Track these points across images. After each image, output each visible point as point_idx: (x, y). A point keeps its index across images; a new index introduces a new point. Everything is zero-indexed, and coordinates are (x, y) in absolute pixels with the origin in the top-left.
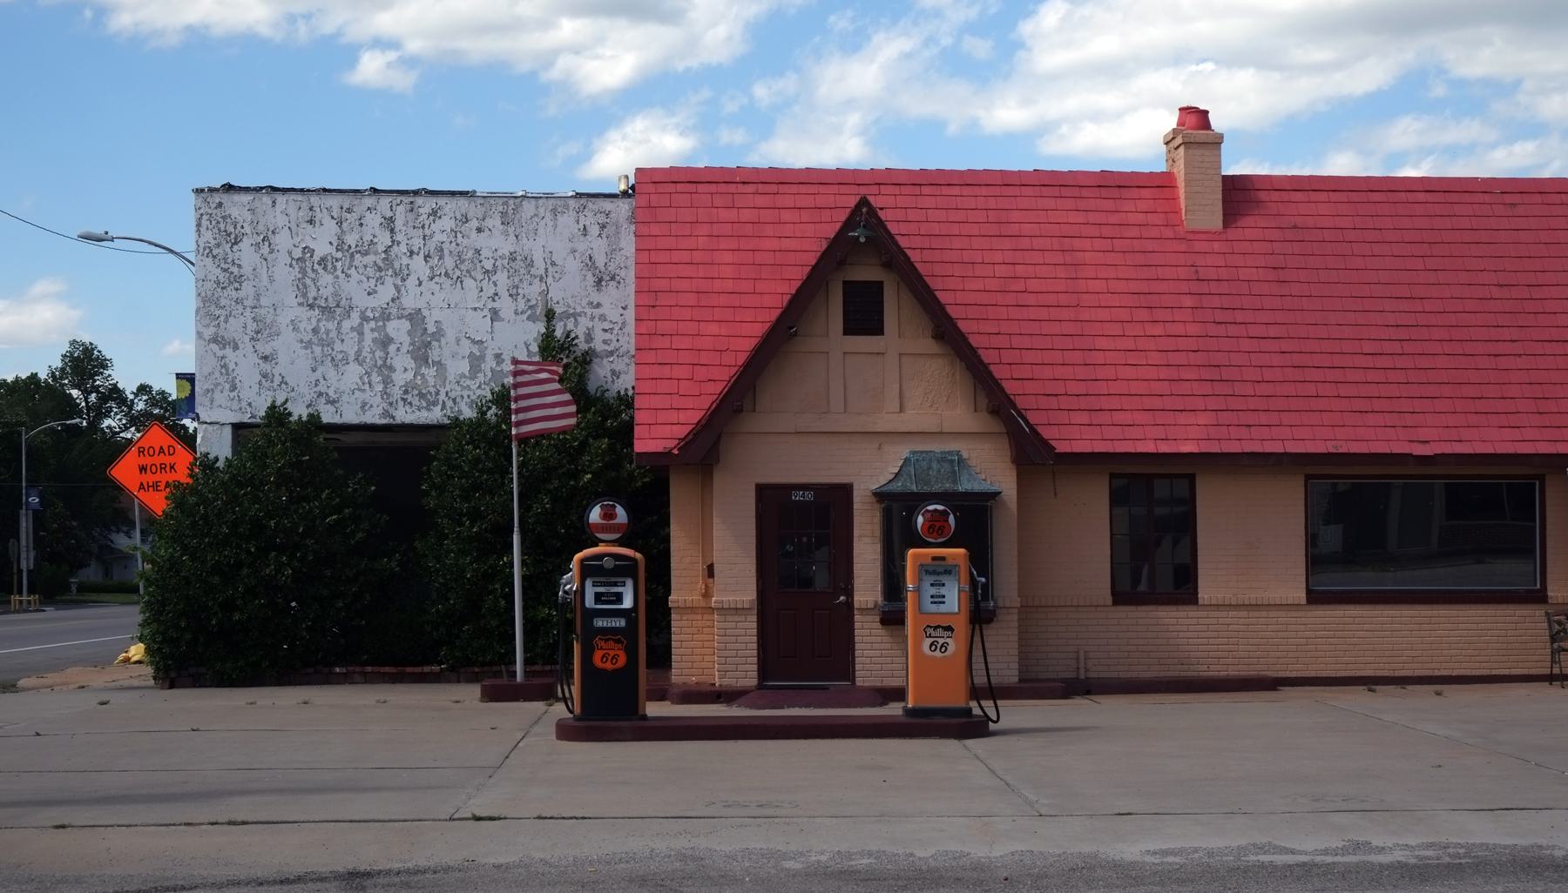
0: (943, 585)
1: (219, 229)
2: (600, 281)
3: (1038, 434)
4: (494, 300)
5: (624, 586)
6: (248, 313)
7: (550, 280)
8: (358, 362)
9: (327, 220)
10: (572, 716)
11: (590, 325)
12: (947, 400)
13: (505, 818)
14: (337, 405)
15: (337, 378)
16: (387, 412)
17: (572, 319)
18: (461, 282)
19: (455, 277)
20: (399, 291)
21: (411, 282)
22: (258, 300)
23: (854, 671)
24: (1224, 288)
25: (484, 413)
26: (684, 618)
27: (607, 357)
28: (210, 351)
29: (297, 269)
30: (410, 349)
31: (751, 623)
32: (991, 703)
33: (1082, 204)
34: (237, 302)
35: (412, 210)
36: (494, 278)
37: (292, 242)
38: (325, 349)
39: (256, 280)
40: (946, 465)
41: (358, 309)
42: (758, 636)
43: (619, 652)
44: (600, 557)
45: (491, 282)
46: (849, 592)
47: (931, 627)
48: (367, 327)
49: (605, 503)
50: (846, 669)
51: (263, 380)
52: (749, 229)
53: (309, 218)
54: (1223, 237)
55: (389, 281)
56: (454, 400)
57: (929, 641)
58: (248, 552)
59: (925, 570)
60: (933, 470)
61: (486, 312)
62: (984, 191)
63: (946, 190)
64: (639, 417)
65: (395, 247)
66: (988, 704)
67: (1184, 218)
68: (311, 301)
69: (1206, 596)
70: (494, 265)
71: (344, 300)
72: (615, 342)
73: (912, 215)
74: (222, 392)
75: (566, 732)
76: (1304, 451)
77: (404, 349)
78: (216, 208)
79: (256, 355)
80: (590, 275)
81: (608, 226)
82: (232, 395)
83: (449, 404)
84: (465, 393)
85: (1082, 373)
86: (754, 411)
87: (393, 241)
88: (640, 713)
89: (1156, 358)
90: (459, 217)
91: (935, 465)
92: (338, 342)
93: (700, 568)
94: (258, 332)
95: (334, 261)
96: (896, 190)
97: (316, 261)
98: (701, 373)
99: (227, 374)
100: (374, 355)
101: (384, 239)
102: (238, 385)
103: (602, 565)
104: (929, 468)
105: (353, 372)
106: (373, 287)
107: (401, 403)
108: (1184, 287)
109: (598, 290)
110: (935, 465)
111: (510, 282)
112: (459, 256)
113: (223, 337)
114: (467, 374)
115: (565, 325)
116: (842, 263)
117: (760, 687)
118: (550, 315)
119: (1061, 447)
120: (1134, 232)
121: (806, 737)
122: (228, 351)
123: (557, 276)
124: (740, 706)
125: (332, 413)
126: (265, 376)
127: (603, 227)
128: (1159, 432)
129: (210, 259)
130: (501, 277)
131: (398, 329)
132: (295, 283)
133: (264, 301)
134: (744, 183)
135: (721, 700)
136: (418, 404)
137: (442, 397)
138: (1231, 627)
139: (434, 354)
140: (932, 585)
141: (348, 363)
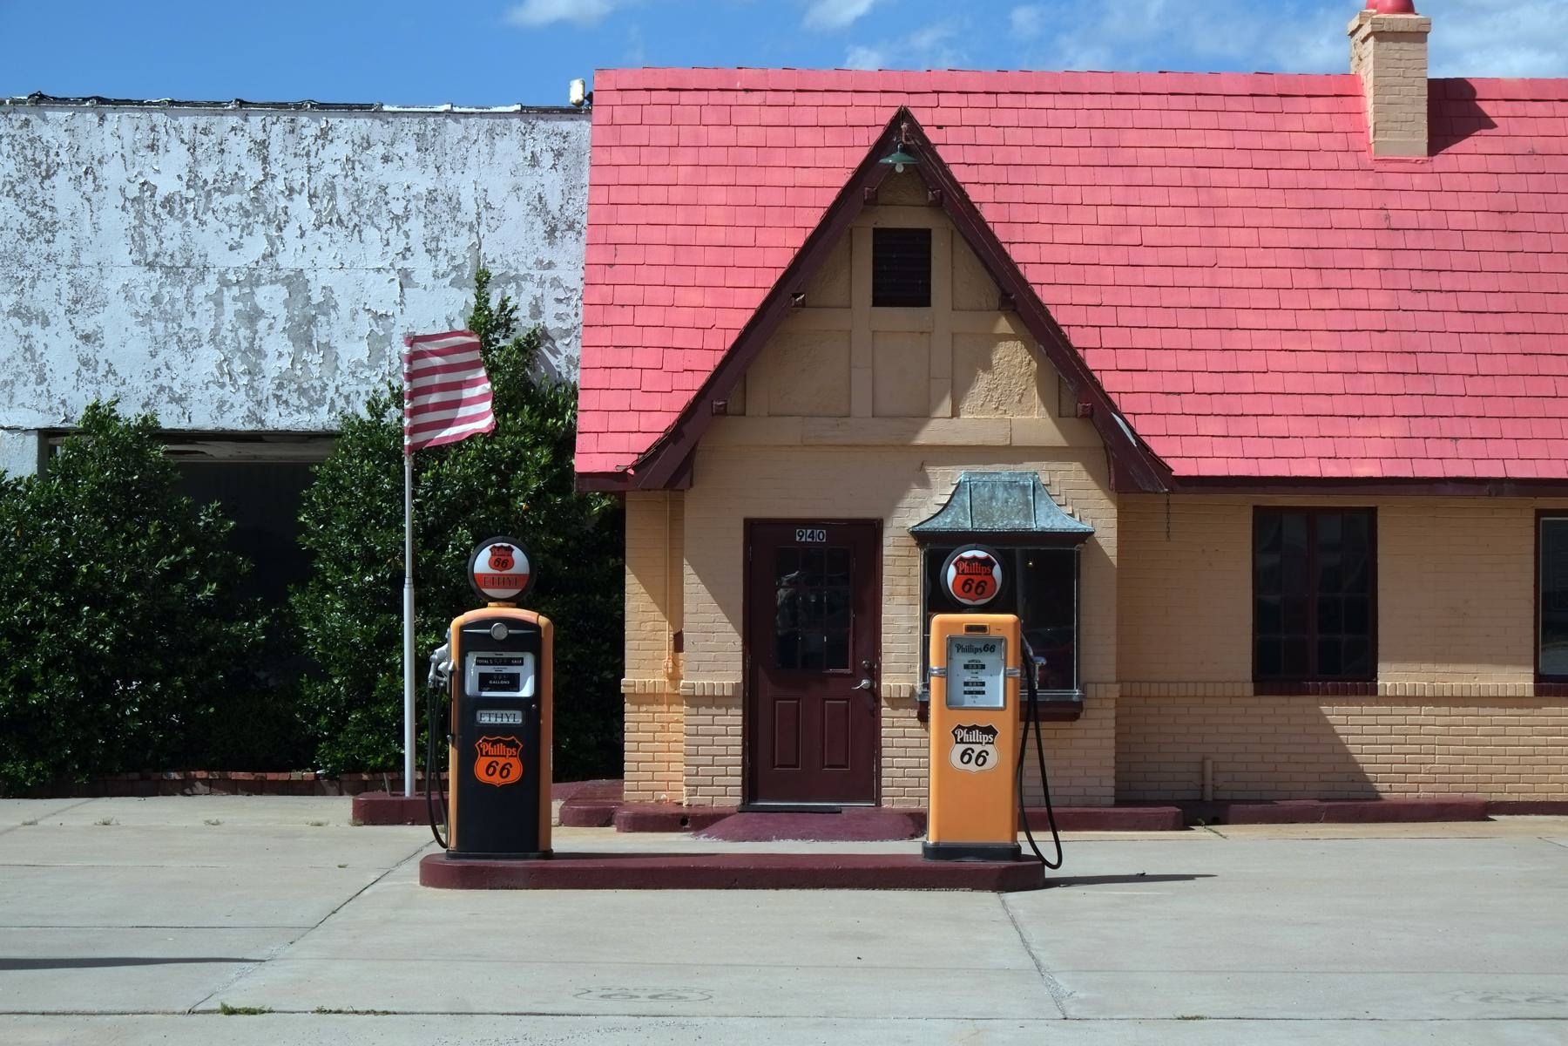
0: (983, 667)
1: (25, 158)
2: (553, 230)
3: (1147, 449)
4: (404, 258)
5: (522, 664)
6: (63, 275)
7: (483, 230)
8: (215, 343)
9: (174, 144)
10: (444, 850)
11: (538, 292)
12: (1020, 401)
13: (270, 1011)
14: (184, 404)
15: (185, 366)
16: (255, 414)
17: (514, 285)
18: (360, 232)
19: (351, 225)
20: (272, 244)
21: (291, 232)
22: (78, 257)
23: (879, 786)
24: (1427, 240)
25: (380, 415)
26: (644, 708)
27: (562, 338)
28: (9, 328)
29: (133, 214)
30: (287, 326)
31: (733, 720)
32: (1049, 835)
33: (1227, 121)
34: (48, 259)
35: (292, 131)
36: (406, 227)
37: (126, 175)
38: (170, 326)
39: (75, 228)
40: (1016, 493)
41: (216, 270)
42: (744, 735)
43: (510, 760)
44: (486, 623)
45: (401, 231)
46: (874, 674)
47: (963, 728)
48: (228, 295)
49: (498, 545)
50: (866, 784)
51: (83, 369)
52: (750, 156)
53: (150, 142)
54: (1428, 167)
55: (259, 230)
56: (347, 398)
57: (961, 748)
58: (53, 609)
59: (954, 645)
60: (997, 500)
61: (393, 274)
62: (1087, 101)
63: (1032, 101)
64: (583, 422)
65: (269, 183)
66: (1043, 839)
67: (1371, 140)
68: (150, 258)
69: (1389, 684)
70: (406, 208)
71: (197, 255)
72: (573, 317)
73: (983, 136)
74: (25, 385)
75: (434, 874)
76: (1534, 475)
77: (279, 327)
78: (21, 127)
79: (73, 332)
80: (539, 221)
81: (566, 154)
82: (39, 389)
83: (340, 403)
84: (363, 388)
85: (1216, 361)
86: (744, 414)
87: (266, 175)
88: (542, 847)
89: (1325, 341)
90: (358, 140)
91: (1000, 494)
92: (187, 316)
93: (667, 636)
94: (76, 302)
95: (184, 201)
96: (962, 100)
97: (158, 203)
98: (675, 360)
99: (33, 360)
100: (236, 334)
101: (254, 171)
102: (49, 375)
103: (489, 635)
104: (991, 498)
105: (208, 358)
106: (237, 239)
107: (273, 402)
108: (1368, 239)
109: (549, 244)
110: (1000, 494)
111: (428, 233)
112: (358, 196)
113: (28, 309)
114: (366, 361)
115: (503, 293)
116: (873, 201)
117: (746, 807)
118: (482, 281)
119: (1180, 468)
120: (1300, 160)
121: (777, 887)
122: (35, 329)
123: (493, 224)
124: (709, 837)
125: (178, 416)
126: (85, 363)
127: (559, 154)
128: (1326, 448)
129: (12, 199)
130: (416, 226)
131: (271, 298)
132: (129, 234)
133: (86, 258)
134: (746, 90)
135: (687, 826)
136: (297, 403)
137: (330, 393)
138: (1424, 729)
139: (320, 334)
140: (966, 667)
141: (200, 346)
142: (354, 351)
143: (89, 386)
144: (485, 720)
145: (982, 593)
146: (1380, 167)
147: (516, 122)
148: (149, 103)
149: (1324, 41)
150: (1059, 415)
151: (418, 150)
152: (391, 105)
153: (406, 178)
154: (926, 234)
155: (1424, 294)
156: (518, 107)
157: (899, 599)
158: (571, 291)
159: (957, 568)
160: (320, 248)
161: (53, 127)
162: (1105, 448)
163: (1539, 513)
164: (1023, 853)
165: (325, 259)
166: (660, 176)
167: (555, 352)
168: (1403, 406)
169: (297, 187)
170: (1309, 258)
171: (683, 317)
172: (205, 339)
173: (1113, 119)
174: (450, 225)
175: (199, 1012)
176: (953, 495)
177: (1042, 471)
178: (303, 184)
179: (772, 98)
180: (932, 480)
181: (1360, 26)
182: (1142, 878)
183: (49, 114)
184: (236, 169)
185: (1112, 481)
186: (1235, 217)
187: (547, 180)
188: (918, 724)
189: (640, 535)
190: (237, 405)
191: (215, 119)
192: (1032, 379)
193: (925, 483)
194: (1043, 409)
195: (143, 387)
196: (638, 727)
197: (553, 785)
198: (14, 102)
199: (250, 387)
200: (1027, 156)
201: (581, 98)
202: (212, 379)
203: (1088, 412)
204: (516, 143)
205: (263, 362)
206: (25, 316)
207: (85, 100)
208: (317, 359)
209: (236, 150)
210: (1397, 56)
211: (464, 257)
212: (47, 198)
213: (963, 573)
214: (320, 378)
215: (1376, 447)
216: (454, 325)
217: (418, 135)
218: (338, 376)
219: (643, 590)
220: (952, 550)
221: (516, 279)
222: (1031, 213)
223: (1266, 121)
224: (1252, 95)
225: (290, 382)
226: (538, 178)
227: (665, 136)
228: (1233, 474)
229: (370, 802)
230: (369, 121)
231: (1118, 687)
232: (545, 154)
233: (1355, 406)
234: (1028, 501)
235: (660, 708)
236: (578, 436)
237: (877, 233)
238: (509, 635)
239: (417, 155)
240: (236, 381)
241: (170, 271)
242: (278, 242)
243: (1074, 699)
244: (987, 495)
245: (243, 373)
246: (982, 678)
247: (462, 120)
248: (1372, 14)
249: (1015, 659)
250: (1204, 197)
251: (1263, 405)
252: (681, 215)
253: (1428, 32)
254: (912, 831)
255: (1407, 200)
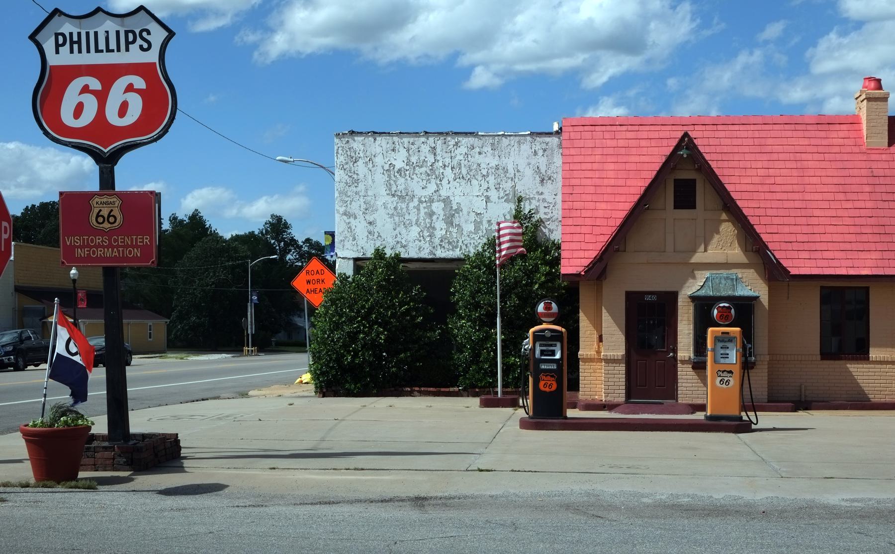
0: (728, 348)
1: (347, 155)
3: (781, 264)
4: (487, 191)
7: (516, 180)
9: (401, 149)
12: (730, 245)
13: (495, 471)
16: (432, 252)
17: (528, 201)
19: (467, 179)
20: (438, 187)
21: (445, 182)
22: (367, 192)
23: (677, 394)
26: (587, 364)
27: (547, 221)
28: (342, 220)
31: (622, 368)
33: (807, 134)
35: (445, 143)
36: (487, 179)
37: (384, 161)
40: (729, 281)
42: (626, 374)
44: (543, 331)
46: (675, 351)
47: (721, 371)
49: (546, 301)
50: (672, 393)
51: (369, 235)
52: (623, 151)
55: (433, 181)
56: (466, 245)
57: (720, 378)
61: (483, 198)
62: (752, 127)
63: (731, 127)
67: (865, 141)
68: (393, 193)
69: (874, 356)
71: (410, 191)
77: (441, 218)
78: (346, 144)
80: (537, 177)
82: (354, 243)
83: (464, 247)
84: (472, 241)
85: (805, 229)
86: (625, 251)
87: (435, 160)
88: (564, 415)
90: (469, 146)
91: (723, 282)
93: (596, 336)
94: (366, 210)
96: (703, 128)
97: (396, 171)
98: (597, 230)
99: (351, 232)
101: (431, 159)
102: (357, 237)
104: (720, 283)
105: (415, 231)
107: (439, 247)
108: (865, 180)
110: (723, 282)
111: (496, 181)
114: (473, 231)
116: (674, 169)
119: (793, 271)
120: (836, 149)
121: (652, 430)
122: (352, 220)
124: (616, 413)
127: (545, 150)
130: (491, 179)
131: (438, 207)
132: (385, 183)
133: (370, 193)
134: (620, 125)
135: (606, 409)
137: (460, 244)
139: (456, 221)
140: (722, 348)
141: (412, 226)
142: (470, 227)
143: (372, 241)
144: (543, 367)
145: (727, 319)
146: (869, 151)
147: (529, 138)
148: (392, 133)
149: (799, 89)
150: (745, 250)
151: (492, 150)
152: (482, 132)
153: (487, 160)
154: (694, 181)
155: (887, 202)
156: (529, 132)
157: (684, 322)
158: (550, 203)
159: (718, 310)
160: (455, 188)
161: (357, 143)
162: (764, 263)
163: (822, 288)
164: (743, 419)
165: (458, 192)
166: (588, 159)
167: (545, 227)
168: (880, 247)
169: (447, 164)
170: (841, 188)
171: (600, 214)
172: (414, 223)
173: (763, 134)
174: (504, 178)
175: (470, 471)
176: (705, 282)
177: (739, 273)
178: (449, 163)
179: (630, 128)
180: (697, 276)
181: (860, 96)
182: (774, 429)
183: (356, 138)
184: (424, 158)
185: (767, 276)
186: (811, 172)
187: (540, 161)
188: (692, 370)
189: (585, 297)
190: (426, 248)
191: (416, 139)
192: (735, 237)
193: (694, 277)
194: (739, 249)
195: (390, 242)
196: (585, 372)
197: (567, 392)
198: (343, 134)
199: (430, 241)
200: (729, 149)
201: (557, 129)
202: (416, 238)
203: (758, 249)
204: (528, 146)
205: (435, 232)
206: (348, 215)
207: (369, 133)
208: (455, 230)
209: (424, 151)
210: (876, 107)
211: (509, 190)
212: (355, 170)
213: (720, 312)
214: (456, 238)
215: (869, 263)
216: (506, 217)
217: (492, 144)
218: (463, 237)
219: (586, 319)
220: (714, 304)
221: (529, 199)
222: (732, 172)
223: (823, 134)
224: (817, 124)
225: (445, 239)
226: (537, 160)
227: (590, 144)
228: (813, 274)
229: (486, 399)
230: (473, 139)
231: (768, 356)
232: (539, 150)
233: (860, 247)
234: (734, 284)
235: (593, 364)
236: (561, 260)
237: (675, 180)
238: (551, 335)
239: (491, 151)
240: (425, 239)
241: (400, 197)
242: (440, 186)
243: (752, 361)
244: (718, 282)
245: (428, 236)
246: (727, 352)
247: (508, 138)
248: (865, 91)
249: (740, 346)
250: (799, 165)
251: (824, 246)
252: (597, 174)
253: (888, 98)
254: (692, 411)
255: (880, 165)
